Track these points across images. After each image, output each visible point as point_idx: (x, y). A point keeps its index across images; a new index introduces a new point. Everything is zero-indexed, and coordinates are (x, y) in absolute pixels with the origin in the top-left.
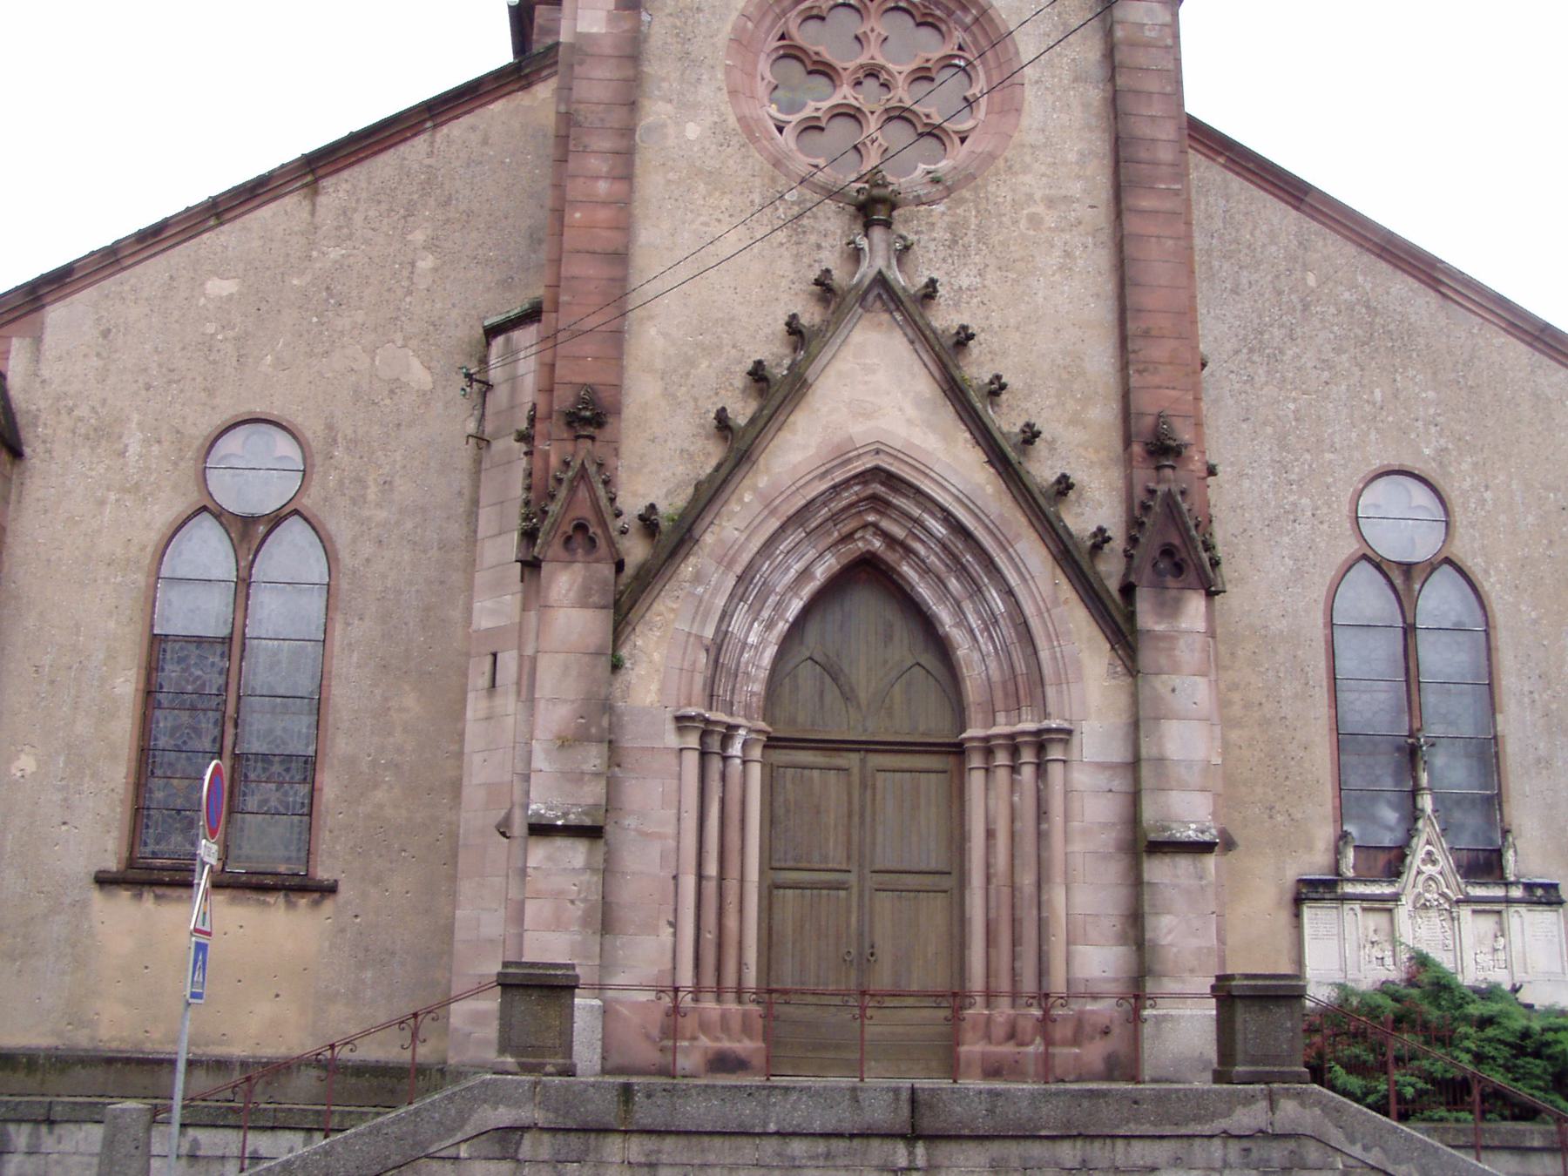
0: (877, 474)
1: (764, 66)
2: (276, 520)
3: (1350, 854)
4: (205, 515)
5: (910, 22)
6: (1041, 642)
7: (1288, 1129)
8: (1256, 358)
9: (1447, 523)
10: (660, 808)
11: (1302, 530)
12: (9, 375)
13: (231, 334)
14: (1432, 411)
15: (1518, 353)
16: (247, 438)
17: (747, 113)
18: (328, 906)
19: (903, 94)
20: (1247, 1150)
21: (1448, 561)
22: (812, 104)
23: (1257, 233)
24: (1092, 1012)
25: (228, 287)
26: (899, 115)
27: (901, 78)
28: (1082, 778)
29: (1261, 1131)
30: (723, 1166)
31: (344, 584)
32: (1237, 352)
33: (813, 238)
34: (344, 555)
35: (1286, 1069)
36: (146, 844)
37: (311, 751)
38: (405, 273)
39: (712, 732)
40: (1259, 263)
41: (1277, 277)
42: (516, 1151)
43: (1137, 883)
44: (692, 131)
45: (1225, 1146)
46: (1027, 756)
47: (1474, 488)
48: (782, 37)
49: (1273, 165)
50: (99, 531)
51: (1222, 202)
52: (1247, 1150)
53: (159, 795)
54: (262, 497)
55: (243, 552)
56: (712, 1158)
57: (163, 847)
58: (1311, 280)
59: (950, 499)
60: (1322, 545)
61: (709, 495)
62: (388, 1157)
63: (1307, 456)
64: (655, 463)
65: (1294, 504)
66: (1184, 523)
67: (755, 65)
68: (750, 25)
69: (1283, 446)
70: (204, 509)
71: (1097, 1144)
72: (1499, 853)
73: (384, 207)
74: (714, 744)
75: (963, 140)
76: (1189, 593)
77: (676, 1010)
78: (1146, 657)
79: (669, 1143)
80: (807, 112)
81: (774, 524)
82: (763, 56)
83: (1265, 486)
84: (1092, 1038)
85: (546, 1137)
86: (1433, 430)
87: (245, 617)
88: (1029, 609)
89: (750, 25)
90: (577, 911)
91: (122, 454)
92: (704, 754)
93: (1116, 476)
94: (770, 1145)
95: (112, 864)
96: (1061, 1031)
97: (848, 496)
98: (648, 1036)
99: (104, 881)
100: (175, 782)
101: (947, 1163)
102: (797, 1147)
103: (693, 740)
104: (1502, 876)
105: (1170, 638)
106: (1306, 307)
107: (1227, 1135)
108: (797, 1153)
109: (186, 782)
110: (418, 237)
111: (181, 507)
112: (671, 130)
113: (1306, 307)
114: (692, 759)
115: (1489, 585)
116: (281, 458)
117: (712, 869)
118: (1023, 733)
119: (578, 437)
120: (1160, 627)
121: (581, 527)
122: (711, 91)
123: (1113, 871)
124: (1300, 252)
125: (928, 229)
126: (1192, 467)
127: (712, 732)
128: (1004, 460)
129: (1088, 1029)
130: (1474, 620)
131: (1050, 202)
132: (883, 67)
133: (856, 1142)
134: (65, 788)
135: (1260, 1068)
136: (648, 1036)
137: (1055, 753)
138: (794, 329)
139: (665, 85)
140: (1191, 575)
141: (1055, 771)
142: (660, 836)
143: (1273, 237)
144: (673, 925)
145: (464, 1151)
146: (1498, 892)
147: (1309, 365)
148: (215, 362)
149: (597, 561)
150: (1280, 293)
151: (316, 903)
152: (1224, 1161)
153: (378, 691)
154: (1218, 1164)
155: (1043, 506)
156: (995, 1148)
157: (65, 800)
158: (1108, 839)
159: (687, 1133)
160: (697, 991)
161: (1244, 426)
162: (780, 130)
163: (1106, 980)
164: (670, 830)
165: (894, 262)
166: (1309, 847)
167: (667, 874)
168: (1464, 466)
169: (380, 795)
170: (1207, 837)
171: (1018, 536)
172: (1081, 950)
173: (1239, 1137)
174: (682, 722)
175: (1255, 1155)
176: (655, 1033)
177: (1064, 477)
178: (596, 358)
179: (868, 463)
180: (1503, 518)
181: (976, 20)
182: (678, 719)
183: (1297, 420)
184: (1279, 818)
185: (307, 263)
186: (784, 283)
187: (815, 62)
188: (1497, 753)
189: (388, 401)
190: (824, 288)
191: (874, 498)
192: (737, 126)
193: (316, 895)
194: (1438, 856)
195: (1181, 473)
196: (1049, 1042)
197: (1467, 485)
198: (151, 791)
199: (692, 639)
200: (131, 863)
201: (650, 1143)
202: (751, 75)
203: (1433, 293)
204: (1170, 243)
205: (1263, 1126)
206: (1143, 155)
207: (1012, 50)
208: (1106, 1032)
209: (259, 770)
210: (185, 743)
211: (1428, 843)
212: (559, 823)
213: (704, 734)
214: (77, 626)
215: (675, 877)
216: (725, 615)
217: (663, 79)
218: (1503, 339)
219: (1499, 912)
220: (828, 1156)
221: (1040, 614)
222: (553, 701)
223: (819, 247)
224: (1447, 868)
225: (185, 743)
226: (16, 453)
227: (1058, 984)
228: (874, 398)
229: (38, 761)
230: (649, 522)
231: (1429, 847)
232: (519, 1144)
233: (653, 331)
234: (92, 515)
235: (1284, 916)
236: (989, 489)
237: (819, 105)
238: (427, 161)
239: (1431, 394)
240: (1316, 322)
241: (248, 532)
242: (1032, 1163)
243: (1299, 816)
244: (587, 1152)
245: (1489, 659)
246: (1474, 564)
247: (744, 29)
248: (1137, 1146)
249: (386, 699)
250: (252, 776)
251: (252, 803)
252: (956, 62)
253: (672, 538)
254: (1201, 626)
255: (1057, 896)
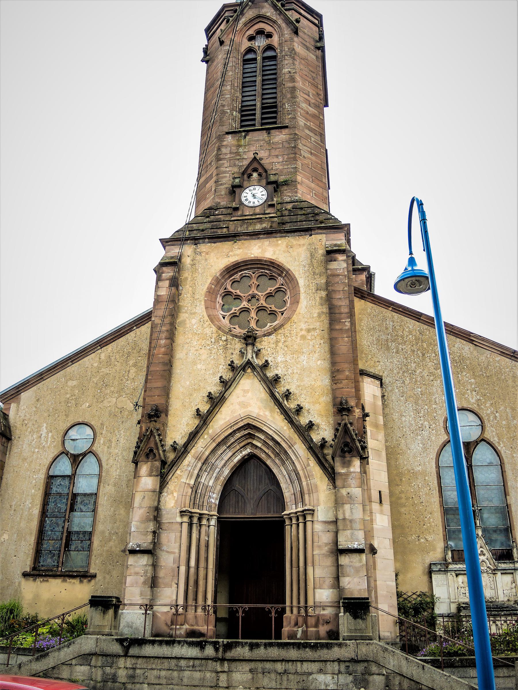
0: (248, 426)
1: (219, 299)
2: (84, 455)
3: (450, 553)
4: (64, 454)
5: (267, 279)
6: (303, 479)
7: (364, 658)
8: (405, 374)
9: (482, 426)
10: (174, 544)
11: (425, 433)
12: (10, 415)
13: (74, 397)
14: (473, 386)
15: (506, 361)
16: (78, 429)
17: (211, 314)
18: (93, 582)
19: (262, 302)
20: (348, 667)
21: (483, 440)
22: (234, 309)
23: (404, 332)
24: (323, 615)
25: (75, 383)
26: (260, 309)
27: (262, 297)
28: (318, 527)
29: (352, 659)
30: (158, 669)
31: (104, 474)
32: (398, 373)
33: (231, 351)
34: (104, 464)
35: (364, 634)
36: (40, 562)
37: (90, 530)
38: (126, 374)
39: (193, 516)
40: (405, 342)
41: (413, 346)
42: (90, 662)
43: (338, 566)
44: (194, 321)
45: (339, 665)
46: (301, 520)
47: (492, 413)
48: (225, 289)
49: (408, 308)
50: (32, 462)
51: (391, 323)
52: (348, 667)
53: (45, 546)
54: (81, 447)
55: (74, 465)
56: (154, 666)
57: (44, 563)
58: (425, 345)
59: (272, 432)
60: (433, 438)
61: (193, 436)
62: (49, 664)
63: (426, 407)
64: (178, 426)
65: (422, 424)
66: (351, 434)
67: (216, 298)
68: (213, 286)
69: (416, 403)
70: (63, 452)
71: (290, 664)
72: (511, 550)
73: (121, 354)
74: (195, 520)
75: (282, 314)
76: (354, 459)
77: (177, 614)
78: (339, 483)
79: (140, 661)
80: (232, 312)
81: (214, 445)
82: (219, 296)
83: (411, 419)
84: (323, 625)
85: (100, 658)
86: (474, 393)
87: (73, 486)
88: (299, 468)
89: (213, 286)
90: (142, 579)
91: (40, 437)
92: (191, 525)
93: (331, 420)
94: (173, 662)
95: (28, 569)
96: (311, 621)
97: (238, 435)
98: (166, 624)
99: (25, 575)
100: (50, 541)
101: (235, 670)
102: (183, 663)
103: (186, 519)
104: (513, 560)
105: (347, 475)
106: (423, 355)
107: (339, 661)
108: (183, 665)
109: (53, 541)
110: (131, 363)
111: (56, 452)
112: (188, 321)
113: (423, 355)
114: (185, 526)
115: (501, 448)
116: (88, 435)
117: (193, 563)
118: (298, 512)
119: (151, 421)
120: (343, 471)
121: (151, 450)
122: (201, 309)
123: (329, 562)
124: (421, 336)
125: (266, 344)
126: (354, 414)
127: (193, 516)
128: (291, 416)
129: (321, 621)
130: (497, 461)
131: (309, 331)
132: (257, 294)
133: (203, 661)
134: (16, 545)
135: (353, 634)
136: (166, 624)
137: (309, 518)
138: (222, 381)
139: (186, 308)
140: (355, 453)
141: (309, 524)
142: (174, 553)
143: (410, 332)
144: (177, 584)
145: (74, 662)
146: (511, 566)
147: (426, 375)
148: (69, 406)
149: (156, 461)
150: (414, 351)
151: (90, 581)
152: (339, 671)
153: (112, 509)
154: (337, 672)
155: (305, 431)
156: (252, 665)
157: (16, 548)
158: (326, 549)
159: (146, 657)
160: (185, 607)
161: (402, 398)
162: (224, 318)
163: (327, 602)
164: (177, 551)
165: (254, 356)
166: (434, 550)
167: (176, 566)
168: (488, 405)
169: (111, 543)
170: (361, 547)
171: (295, 443)
172: (318, 591)
173: (345, 661)
174: (182, 513)
175: (351, 668)
176: (169, 623)
177: (311, 422)
178: (158, 396)
179: (245, 422)
180: (504, 422)
181: (286, 275)
182: (181, 512)
183: (421, 394)
184: (422, 540)
185: (98, 374)
186: (221, 367)
187: (235, 295)
188: (508, 511)
189: (120, 415)
190: (232, 366)
191: (249, 434)
192: (207, 318)
193: (89, 579)
194: (485, 551)
195: (351, 417)
196: (307, 627)
197: (489, 412)
198: (42, 545)
199: (186, 485)
200: (34, 569)
201: (134, 661)
202: (215, 302)
203: (471, 345)
204: (346, 339)
205: (353, 657)
206: (337, 311)
207: (296, 283)
208: (327, 623)
209: (76, 537)
210: (54, 528)
211: (481, 547)
212: (138, 549)
213: (191, 517)
214: (23, 492)
215: (178, 567)
216: (198, 476)
217: (186, 306)
218: (499, 358)
219: (513, 573)
220: (193, 666)
221: (303, 470)
222: (140, 507)
223: (232, 354)
224: (489, 557)
225: (54, 528)
226: (9, 439)
227: (310, 603)
228: (248, 400)
229: (9, 536)
230: (174, 448)
231: (481, 549)
232: (91, 660)
233: (179, 386)
234: (32, 457)
235: (425, 578)
236: (285, 428)
237: (236, 309)
238: (134, 339)
239: (473, 380)
240: (427, 359)
241: (76, 459)
242: (266, 670)
243: (430, 539)
244: (113, 663)
245: (503, 476)
246: (495, 440)
247: (211, 288)
248: (305, 664)
249: (115, 511)
250: (73, 539)
251: (73, 547)
252: (282, 289)
253: (182, 451)
254: (358, 470)
255: (310, 570)
